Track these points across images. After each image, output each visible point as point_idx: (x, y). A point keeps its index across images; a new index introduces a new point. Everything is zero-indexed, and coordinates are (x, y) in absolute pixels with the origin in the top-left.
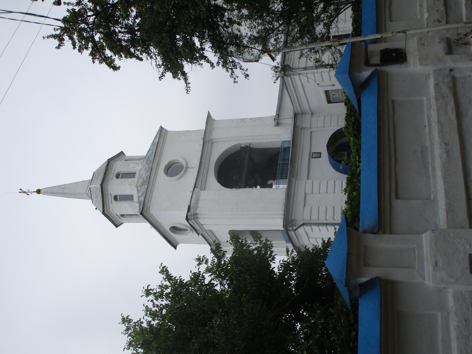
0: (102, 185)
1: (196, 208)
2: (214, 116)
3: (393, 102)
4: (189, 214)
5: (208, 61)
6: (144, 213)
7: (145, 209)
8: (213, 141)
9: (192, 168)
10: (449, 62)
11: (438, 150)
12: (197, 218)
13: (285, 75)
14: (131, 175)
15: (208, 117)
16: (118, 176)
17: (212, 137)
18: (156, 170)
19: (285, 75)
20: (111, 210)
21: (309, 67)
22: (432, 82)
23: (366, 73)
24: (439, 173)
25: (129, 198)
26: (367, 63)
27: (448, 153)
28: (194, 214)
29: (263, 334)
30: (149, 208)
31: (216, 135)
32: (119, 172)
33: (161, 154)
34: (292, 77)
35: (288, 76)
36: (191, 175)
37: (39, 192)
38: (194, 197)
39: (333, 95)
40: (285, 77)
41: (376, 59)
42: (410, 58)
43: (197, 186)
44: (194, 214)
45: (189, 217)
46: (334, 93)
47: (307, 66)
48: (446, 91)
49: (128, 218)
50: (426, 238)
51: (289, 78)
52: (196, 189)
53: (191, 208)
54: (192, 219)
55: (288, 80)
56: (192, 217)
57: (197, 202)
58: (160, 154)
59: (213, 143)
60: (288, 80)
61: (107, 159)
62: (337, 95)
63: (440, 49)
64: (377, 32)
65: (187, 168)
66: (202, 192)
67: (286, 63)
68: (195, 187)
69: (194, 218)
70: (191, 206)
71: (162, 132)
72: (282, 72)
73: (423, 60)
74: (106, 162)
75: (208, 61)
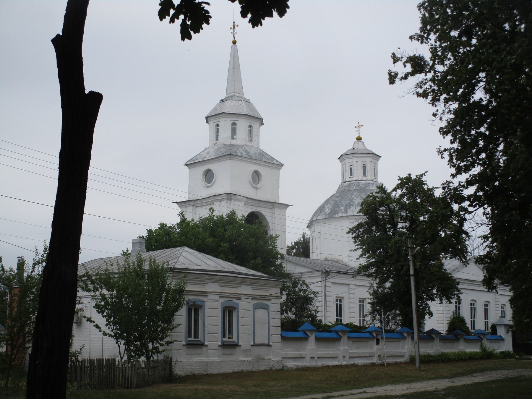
0: (246, 115)
1: (234, 200)
2: (289, 211)
3: (368, 341)
4: (232, 195)
6: (230, 156)
7: (233, 157)
8: (273, 209)
9: (256, 192)
10: (376, 356)
11: (360, 351)
12: (228, 200)
13: (323, 272)
16: (250, 126)
17: (276, 209)
18: (257, 163)
19: (323, 272)
20: (225, 119)
21: (326, 288)
22: (372, 351)
23: (375, 335)
24: (356, 351)
26: (377, 335)
27: (360, 354)
28: (231, 198)
30: (232, 159)
31: (277, 211)
32: (252, 127)
33: (265, 166)
34: (320, 277)
35: (322, 274)
36: (251, 193)
37: (234, 42)
38: (242, 197)
41: (377, 338)
42: (377, 346)
43: (247, 199)
44: (231, 198)
45: (230, 195)
47: (327, 287)
48: (371, 354)
49: (214, 130)
50: (347, 348)
51: (320, 275)
52: (245, 199)
53: (235, 196)
54: (228, 196)
55: (319, 274)
56: (229, 197)
57: (238, 200)
58: (266, 165)
59: (272, 209)
60: (319, 274)
61: (263, 117)
63: (379, 354)
64: (385, 338)
65: (256, 188)
66: (243, 203)
67: (330, 273)
68: (247, 198)
69: (228, 198)
70: (237, 196)
71: (281, 165)
72: (325, 271)
73: (377, 349)
74: (261, 117)
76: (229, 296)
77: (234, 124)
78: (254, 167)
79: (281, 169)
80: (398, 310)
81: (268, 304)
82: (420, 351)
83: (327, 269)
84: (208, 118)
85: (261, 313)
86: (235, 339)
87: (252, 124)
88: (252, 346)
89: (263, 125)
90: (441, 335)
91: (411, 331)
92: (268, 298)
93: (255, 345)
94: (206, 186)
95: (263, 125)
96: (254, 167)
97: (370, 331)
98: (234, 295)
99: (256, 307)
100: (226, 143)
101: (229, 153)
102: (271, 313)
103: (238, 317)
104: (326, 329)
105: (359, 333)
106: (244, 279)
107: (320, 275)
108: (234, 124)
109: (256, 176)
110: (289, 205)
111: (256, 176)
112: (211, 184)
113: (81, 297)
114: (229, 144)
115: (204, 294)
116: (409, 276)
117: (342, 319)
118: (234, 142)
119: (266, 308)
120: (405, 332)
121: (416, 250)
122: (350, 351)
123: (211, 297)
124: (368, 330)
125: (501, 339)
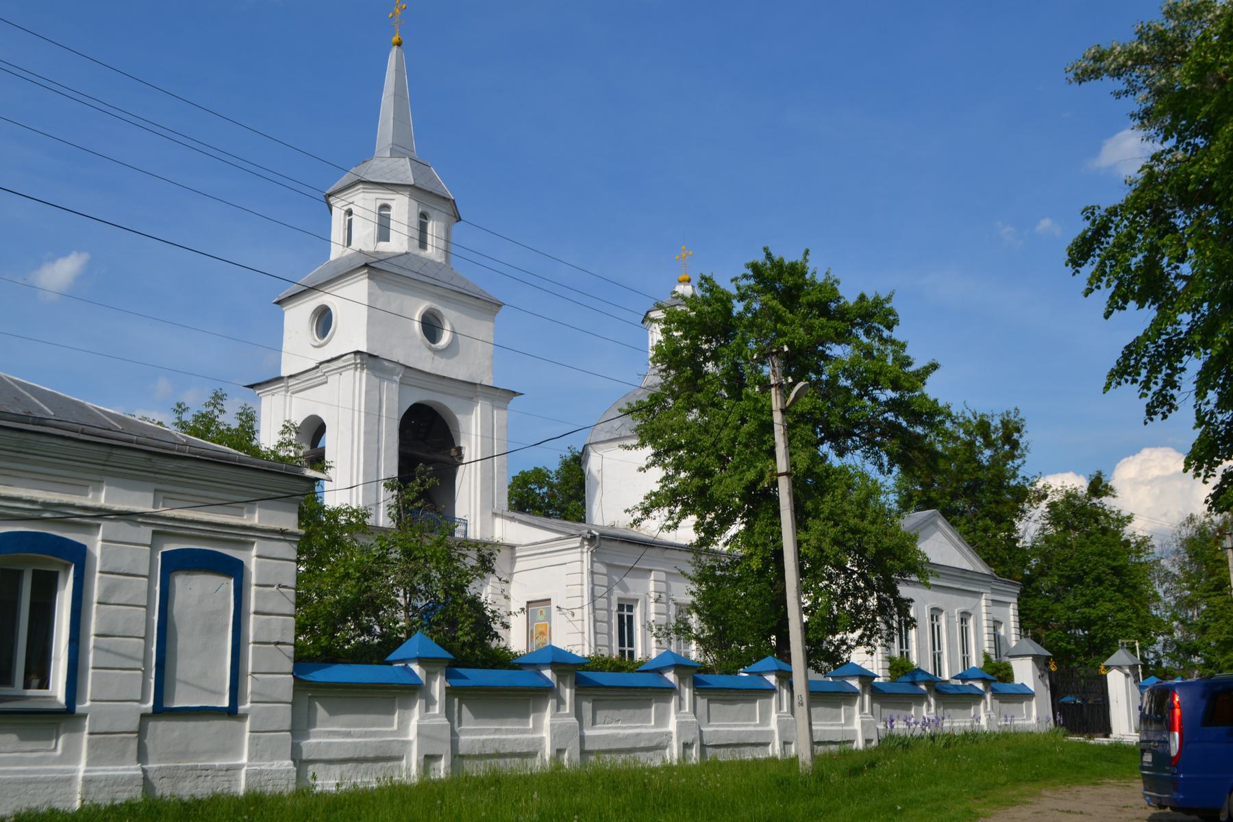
5: (1046, 797)
13: (584, 539)
14: (423, 244)
15: (514, 392)
25: (384, 233)
29: (1150, 773)
36: (426, 361)
38: (391, 365)
39: (541, 611)
40: (580, 539)
43: (408, 370)
46: (544, 613)
51: (578, 545)
52: (403, 368)
54: (355, 359)
62: (540, 618)
64: (95, 647)
72: (589, 536)
75: (1046, 797)
76: (36, 514)
77: (385, 207)
79: (497, 312)
82: (814, 728)
83: (593, 532)
87: (429, 211)
91: (784, 666)
92: (242, 538)
94: (316, 344)
97: (659, 666)
98: (57, 509)
99: (175, 564)
100: (365, 249)
105: (512, 671)
106: (115, 451)
107: (578, 545)
109: (431, 327)
110: (514, 393)
111: (431, 327)
112: (326, 339)
118: (383, 247)
120: (769, 672)
125: (1024, 695)
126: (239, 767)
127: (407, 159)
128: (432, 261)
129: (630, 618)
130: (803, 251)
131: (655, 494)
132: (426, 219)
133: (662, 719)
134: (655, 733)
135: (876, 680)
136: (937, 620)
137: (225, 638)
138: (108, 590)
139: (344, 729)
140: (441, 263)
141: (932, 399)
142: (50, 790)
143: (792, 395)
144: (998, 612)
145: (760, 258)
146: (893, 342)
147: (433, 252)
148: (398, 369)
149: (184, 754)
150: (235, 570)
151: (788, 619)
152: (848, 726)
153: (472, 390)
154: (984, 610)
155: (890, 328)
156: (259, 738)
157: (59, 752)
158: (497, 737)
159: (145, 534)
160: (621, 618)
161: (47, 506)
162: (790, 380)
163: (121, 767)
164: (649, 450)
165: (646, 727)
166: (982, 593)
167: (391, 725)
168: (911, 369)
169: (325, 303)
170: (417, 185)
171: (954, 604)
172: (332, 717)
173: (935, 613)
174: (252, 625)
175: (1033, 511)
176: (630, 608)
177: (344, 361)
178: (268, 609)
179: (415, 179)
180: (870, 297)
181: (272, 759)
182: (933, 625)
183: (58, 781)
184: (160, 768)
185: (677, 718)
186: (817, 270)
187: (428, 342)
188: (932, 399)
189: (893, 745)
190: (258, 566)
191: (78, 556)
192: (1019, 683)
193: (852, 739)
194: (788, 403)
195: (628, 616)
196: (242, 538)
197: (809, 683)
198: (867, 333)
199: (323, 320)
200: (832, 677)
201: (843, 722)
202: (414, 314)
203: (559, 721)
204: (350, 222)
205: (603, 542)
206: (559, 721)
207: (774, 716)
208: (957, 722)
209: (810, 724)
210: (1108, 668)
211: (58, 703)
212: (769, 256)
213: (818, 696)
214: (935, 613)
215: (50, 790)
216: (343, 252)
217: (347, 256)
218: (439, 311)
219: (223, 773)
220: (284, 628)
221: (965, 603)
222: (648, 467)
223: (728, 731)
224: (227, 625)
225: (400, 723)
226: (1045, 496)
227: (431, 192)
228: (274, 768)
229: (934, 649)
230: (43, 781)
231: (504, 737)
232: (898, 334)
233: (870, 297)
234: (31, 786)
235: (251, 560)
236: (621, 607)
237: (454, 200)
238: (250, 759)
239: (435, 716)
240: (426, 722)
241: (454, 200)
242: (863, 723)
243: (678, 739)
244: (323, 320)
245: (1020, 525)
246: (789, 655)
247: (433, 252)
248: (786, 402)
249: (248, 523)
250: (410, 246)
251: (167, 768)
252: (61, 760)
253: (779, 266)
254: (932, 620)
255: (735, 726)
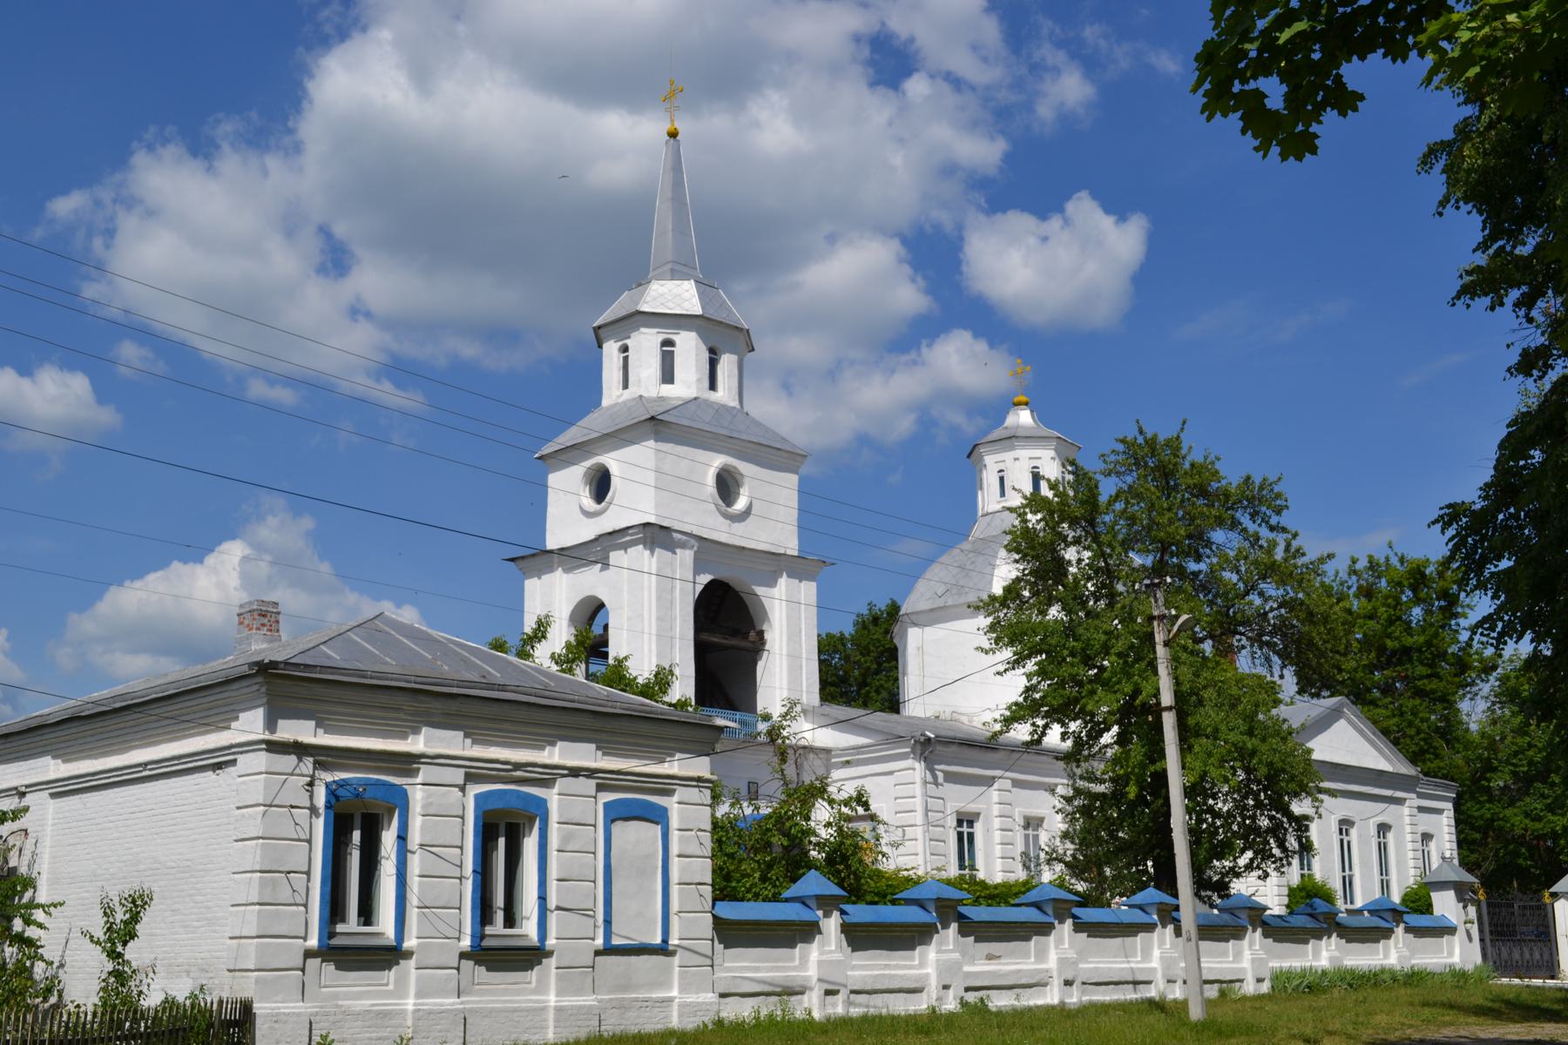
6: (653, 423)
14: (713, 386)
25: (668, 376)
36: (720, 530)
38: (684, 538)
45: (649, 529)
72: (922, 739)
77: (668, 343)
78: (718, 461)
80: (1320, 59)
81: (665, 805)
82: (1202, 965)
83: (928, 733)
84: (600, 331)
85: (635, 837)
86: (529, 929)
88: (598, 953)
89: (753, 350)
90: (1268, 912)
91: (1168, 899)
92: (665, 786)
93: (609, 950)
95: (753, 350)
96: (718, 461)
99: (616, 814)
101: (648, 416)
102: (675, 836)
103: (402, 838)
104: (891, 889)
108: (668, 343)
109: (727, 485)
111: (727, 485)
112: (603, 504)
113: (23, 789)
114: (655, 395)
115: (407, 763)
116: (1158, 710)
117: (960, 869)
118: (667, 390)
119: (658, 817)
121: (1180, 621)
122: (967, 969)
123: (426, 772)
124: (1033, 896)
126: (671, 1000)
127: (692, 282)
128: (724, 406)
129: (971, 836)
130: (1181, 421)
131: (1016, 704)
132: (715, 354)
133: (1041, 955)
134: (1035, 970)
135: (1268, 912)
136: (1347, 835)
137: (656, 880)
138: (566, 839)
139: (753, 965)
140: (734, 408)
141: (1445, 176)
142: (530, 1018)
143: (1176, 628)
144: (1426, 822)
145: (1131, 433)
146: (1284, 530)
147: (725, 394)
148: (693, 541)
149: (626, 988)
150: (658, 817)
151: (1174, 855)
152: (1238, 963)
153: (774, 564)
154: (1407, 820)
155: (1278, 511)
156: (687, 972)
157: (534, 985)
158: (886, 972)
159: (591, 785)
160: (960, 835)
161: (518, 766)
162: (1173, 612)
163: (581, 998)
164: (1007, 653)
165: (1026, 963)
166: (1405, 799)
167: (793, 959)
168: (1300, 561)
169: (608, 466)
170: (706, 315)
171: (1367, 814)
172: (338, 972)
173: (1345, 825)
174: (675, 863)
175: (1481, 685)
176: (971, 823)
177: (631, 535)
178: (689, 852)
179: (703, 308)
180: (1257, 480)
181: (697, 993)
182: (1342, 841)
183: (535, 1010)
184: (611, 1000)
185: (1057, 954)
186: (1195, 450)
187: (720, 502)
188: (1445, 176)
189: (1289, 987)
190: (680, 812)
191: (539, 811)
192: (1439, 914)
193: (1241, 977)
194: (1171, 636)
195: (968, 833)
196: (665, 786)
197: (1197, 916)
198: (1253, 516)
199: (601, 484)
200: (1219, 910)
201: (1231, 959)
202: (705, 475)
203: (944, 957)
204: (626, 359)
205: (939, 748)
206: (944, 957)
207: (1156, 953)
208: (1363, 958)
209: (1199, 960)
210: (1555, 896)
211: (531, 940)
212: (1141, 432)
213: (1210, 932)
214: (1345, 825)
215: (530, 1018)
216: (618, 397)
217: (625, 403)
218: (735, 468)
219: (658, 1004)
220: (703, 870)
221: (1387, 813)
222: (1006, 671)
223: (1109, 968)
224: (657, 868)
225: (539, 981)
226: (1495, 668)
227: (721, 323)
228: (700, 1000)
229: (1344, 871)
230: (523, 1010)
231: (893, 972)
232: (1285, 519)
233: (1257, 480)
234: (516, 1014)
235: (672, 804)
236: (960, 823)
237: (748, 331)
238: (681, 991)
239: (831, 952)
240: (824, 957)
241: (748, 331)
242: (1253, 960)
243: (1060, 975)
244: (601, 484)
245: (1464, 706)
246: (1177, 890)
247: (725, 394)
248: (1169, 631)
249: (670, 772)
250: (698, 389)
251: (617, 999)
252: (536, 991)
253: (1152, 443)
254: (1341, 833)
255: (1116, 962)
